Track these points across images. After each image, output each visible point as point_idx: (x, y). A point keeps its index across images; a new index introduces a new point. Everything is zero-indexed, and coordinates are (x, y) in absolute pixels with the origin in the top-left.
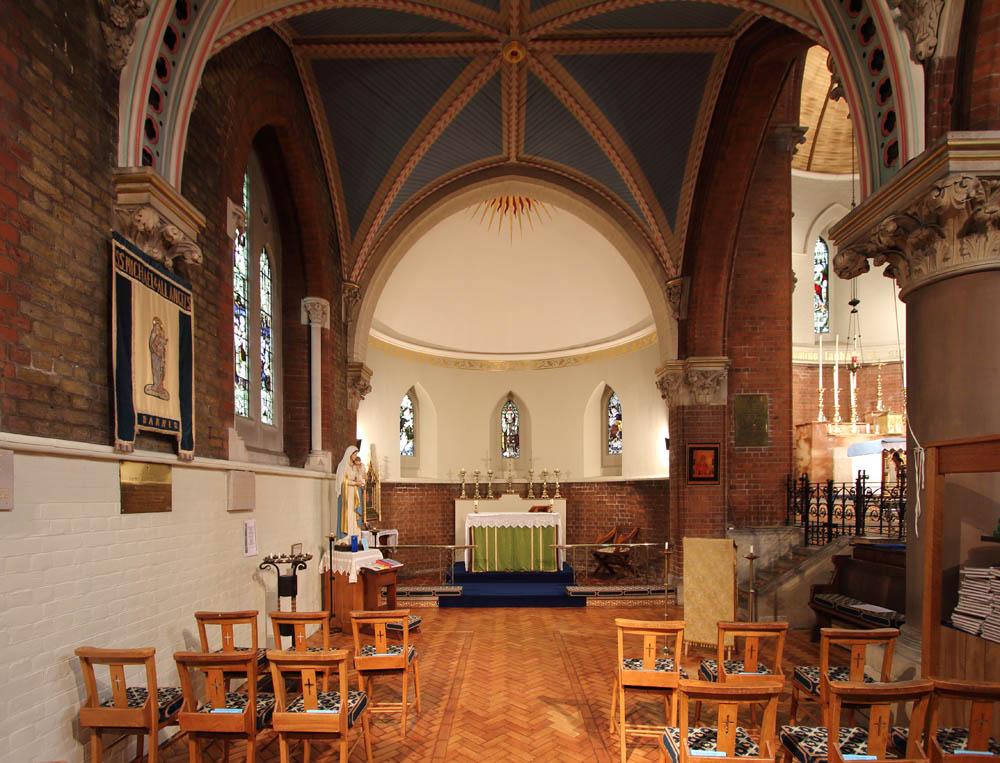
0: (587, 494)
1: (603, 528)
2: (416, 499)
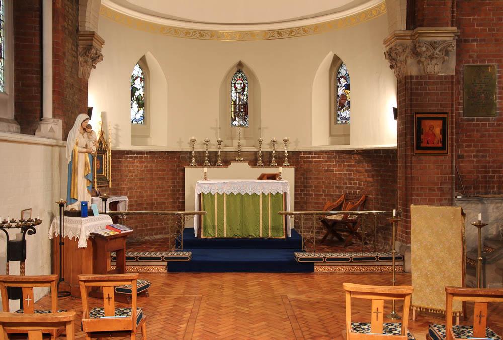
0: (315, 162)
1: (332, 196)
2: (146, 167)
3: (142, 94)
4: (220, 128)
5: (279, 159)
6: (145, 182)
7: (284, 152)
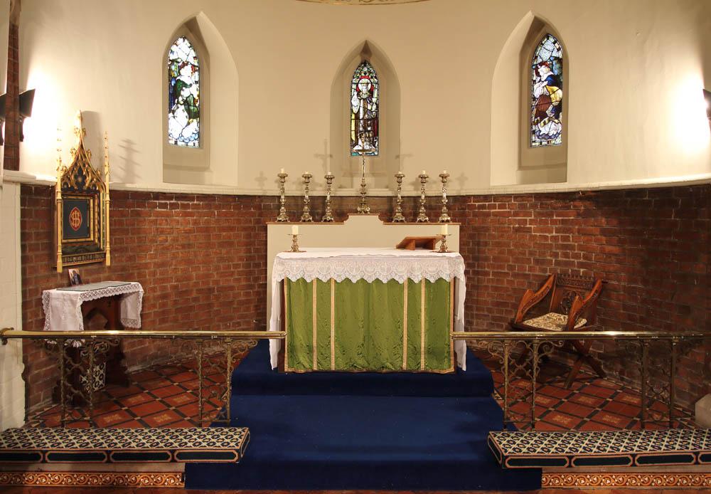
0: (496, 215)
1: (527, 276)
2: (195, 223)
3: (196, 95)
4: (331, 156)
5: (430, 209)
6: (195, 252)
7: (442, 197)
